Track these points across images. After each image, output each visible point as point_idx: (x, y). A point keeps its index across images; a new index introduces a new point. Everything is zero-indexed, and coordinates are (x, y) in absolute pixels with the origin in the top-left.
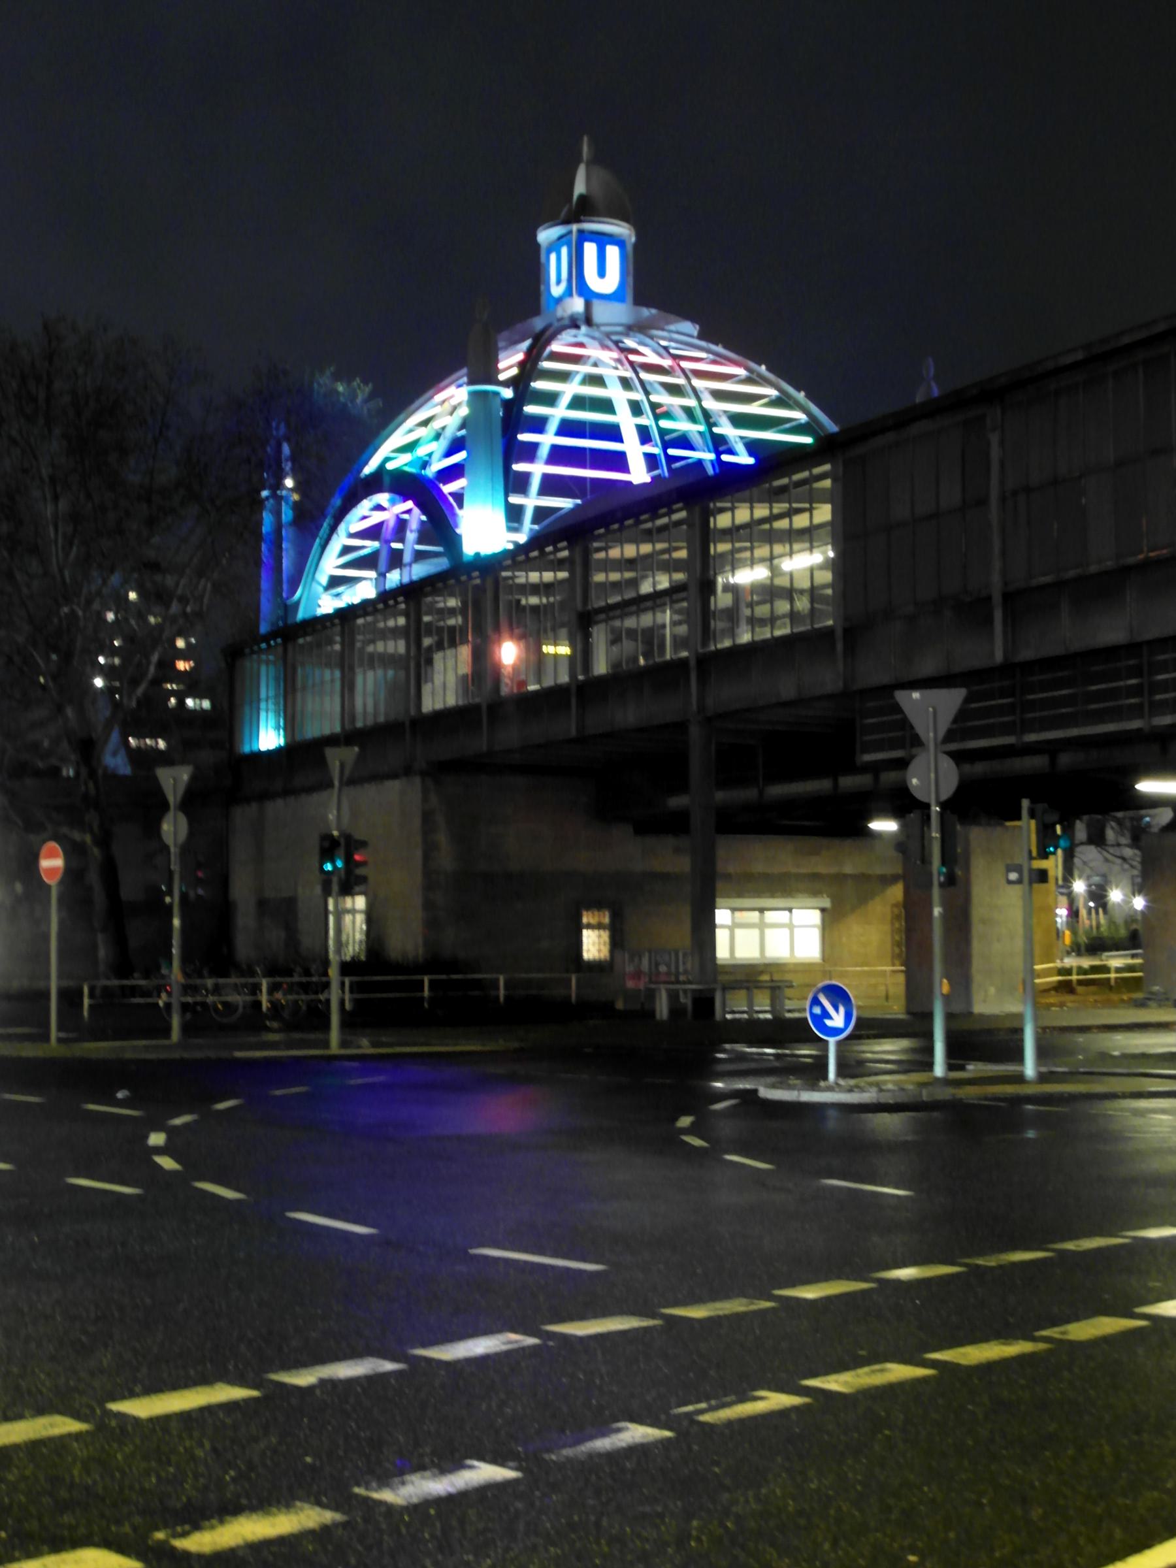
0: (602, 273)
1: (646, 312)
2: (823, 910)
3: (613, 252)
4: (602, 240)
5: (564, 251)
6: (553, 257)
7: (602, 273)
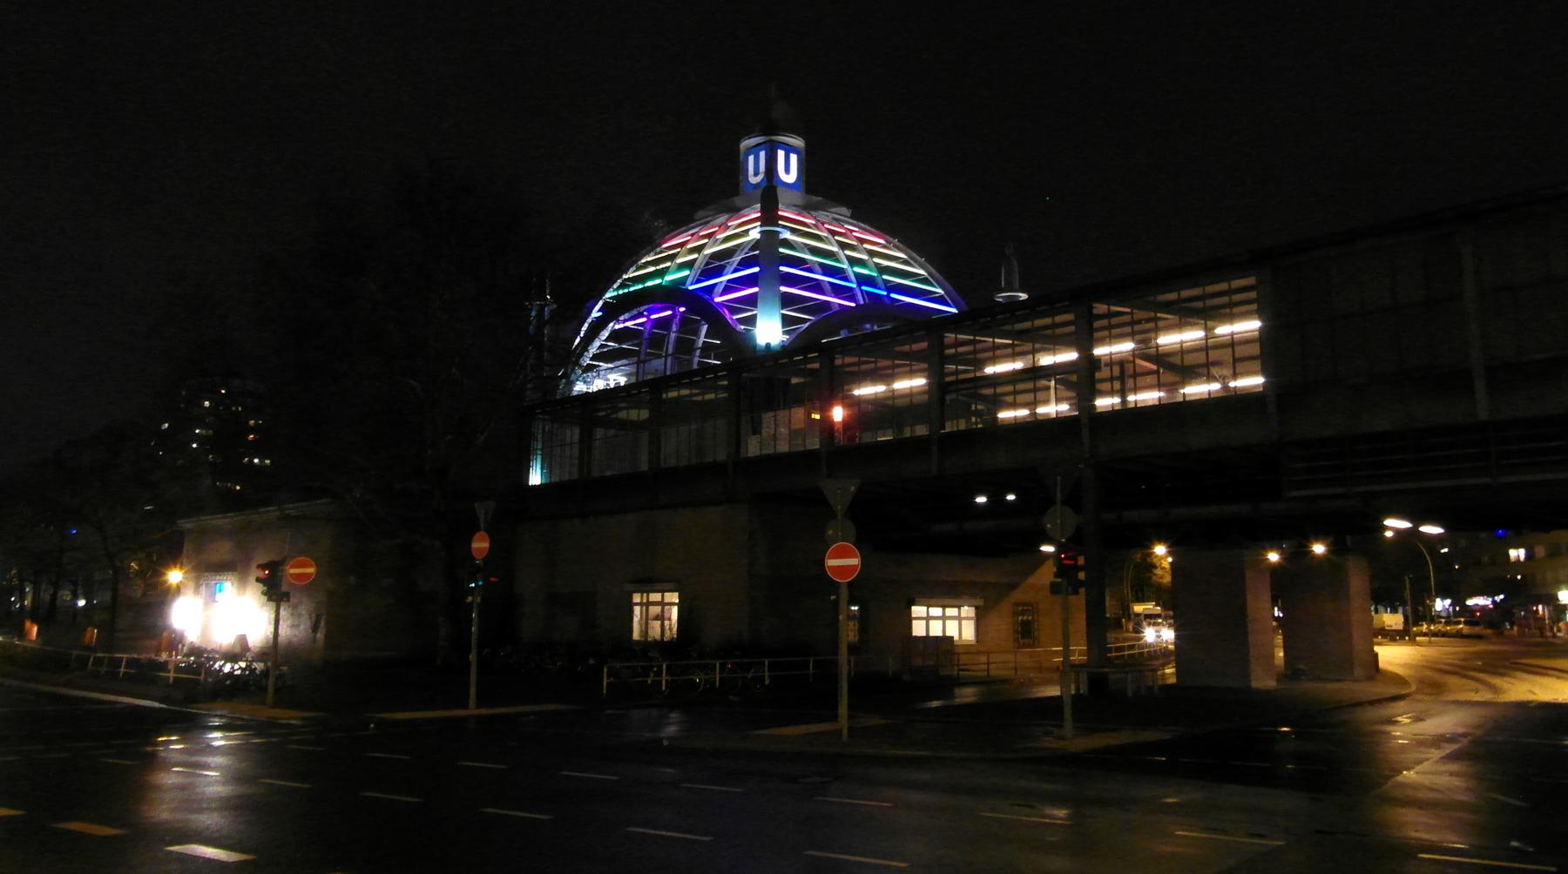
0: (787, 171)
1: (815, 199)
2: (977, 608)
3: (794, 158)
4: (790, 150)
5: (762, 154)
6: (751, 158)
7: (787, 171)
